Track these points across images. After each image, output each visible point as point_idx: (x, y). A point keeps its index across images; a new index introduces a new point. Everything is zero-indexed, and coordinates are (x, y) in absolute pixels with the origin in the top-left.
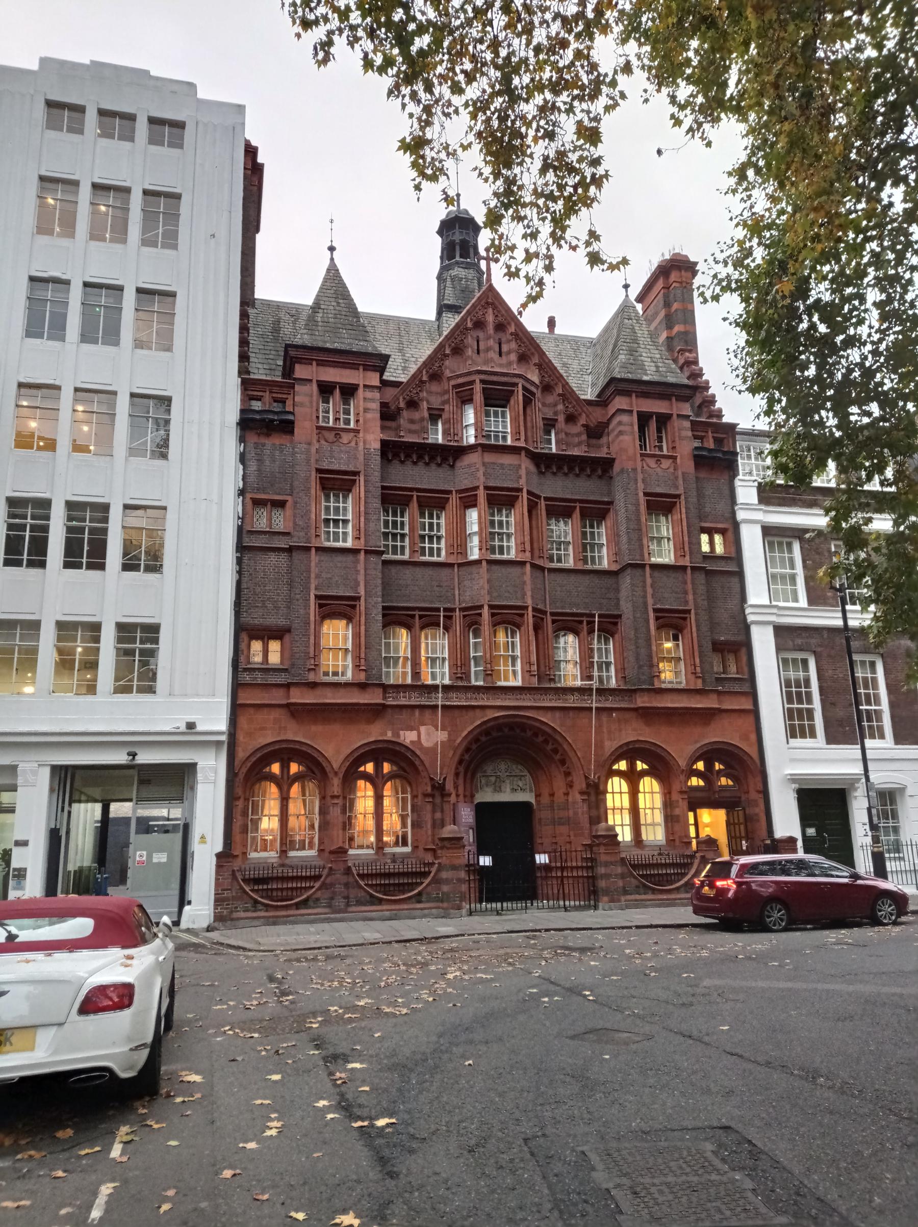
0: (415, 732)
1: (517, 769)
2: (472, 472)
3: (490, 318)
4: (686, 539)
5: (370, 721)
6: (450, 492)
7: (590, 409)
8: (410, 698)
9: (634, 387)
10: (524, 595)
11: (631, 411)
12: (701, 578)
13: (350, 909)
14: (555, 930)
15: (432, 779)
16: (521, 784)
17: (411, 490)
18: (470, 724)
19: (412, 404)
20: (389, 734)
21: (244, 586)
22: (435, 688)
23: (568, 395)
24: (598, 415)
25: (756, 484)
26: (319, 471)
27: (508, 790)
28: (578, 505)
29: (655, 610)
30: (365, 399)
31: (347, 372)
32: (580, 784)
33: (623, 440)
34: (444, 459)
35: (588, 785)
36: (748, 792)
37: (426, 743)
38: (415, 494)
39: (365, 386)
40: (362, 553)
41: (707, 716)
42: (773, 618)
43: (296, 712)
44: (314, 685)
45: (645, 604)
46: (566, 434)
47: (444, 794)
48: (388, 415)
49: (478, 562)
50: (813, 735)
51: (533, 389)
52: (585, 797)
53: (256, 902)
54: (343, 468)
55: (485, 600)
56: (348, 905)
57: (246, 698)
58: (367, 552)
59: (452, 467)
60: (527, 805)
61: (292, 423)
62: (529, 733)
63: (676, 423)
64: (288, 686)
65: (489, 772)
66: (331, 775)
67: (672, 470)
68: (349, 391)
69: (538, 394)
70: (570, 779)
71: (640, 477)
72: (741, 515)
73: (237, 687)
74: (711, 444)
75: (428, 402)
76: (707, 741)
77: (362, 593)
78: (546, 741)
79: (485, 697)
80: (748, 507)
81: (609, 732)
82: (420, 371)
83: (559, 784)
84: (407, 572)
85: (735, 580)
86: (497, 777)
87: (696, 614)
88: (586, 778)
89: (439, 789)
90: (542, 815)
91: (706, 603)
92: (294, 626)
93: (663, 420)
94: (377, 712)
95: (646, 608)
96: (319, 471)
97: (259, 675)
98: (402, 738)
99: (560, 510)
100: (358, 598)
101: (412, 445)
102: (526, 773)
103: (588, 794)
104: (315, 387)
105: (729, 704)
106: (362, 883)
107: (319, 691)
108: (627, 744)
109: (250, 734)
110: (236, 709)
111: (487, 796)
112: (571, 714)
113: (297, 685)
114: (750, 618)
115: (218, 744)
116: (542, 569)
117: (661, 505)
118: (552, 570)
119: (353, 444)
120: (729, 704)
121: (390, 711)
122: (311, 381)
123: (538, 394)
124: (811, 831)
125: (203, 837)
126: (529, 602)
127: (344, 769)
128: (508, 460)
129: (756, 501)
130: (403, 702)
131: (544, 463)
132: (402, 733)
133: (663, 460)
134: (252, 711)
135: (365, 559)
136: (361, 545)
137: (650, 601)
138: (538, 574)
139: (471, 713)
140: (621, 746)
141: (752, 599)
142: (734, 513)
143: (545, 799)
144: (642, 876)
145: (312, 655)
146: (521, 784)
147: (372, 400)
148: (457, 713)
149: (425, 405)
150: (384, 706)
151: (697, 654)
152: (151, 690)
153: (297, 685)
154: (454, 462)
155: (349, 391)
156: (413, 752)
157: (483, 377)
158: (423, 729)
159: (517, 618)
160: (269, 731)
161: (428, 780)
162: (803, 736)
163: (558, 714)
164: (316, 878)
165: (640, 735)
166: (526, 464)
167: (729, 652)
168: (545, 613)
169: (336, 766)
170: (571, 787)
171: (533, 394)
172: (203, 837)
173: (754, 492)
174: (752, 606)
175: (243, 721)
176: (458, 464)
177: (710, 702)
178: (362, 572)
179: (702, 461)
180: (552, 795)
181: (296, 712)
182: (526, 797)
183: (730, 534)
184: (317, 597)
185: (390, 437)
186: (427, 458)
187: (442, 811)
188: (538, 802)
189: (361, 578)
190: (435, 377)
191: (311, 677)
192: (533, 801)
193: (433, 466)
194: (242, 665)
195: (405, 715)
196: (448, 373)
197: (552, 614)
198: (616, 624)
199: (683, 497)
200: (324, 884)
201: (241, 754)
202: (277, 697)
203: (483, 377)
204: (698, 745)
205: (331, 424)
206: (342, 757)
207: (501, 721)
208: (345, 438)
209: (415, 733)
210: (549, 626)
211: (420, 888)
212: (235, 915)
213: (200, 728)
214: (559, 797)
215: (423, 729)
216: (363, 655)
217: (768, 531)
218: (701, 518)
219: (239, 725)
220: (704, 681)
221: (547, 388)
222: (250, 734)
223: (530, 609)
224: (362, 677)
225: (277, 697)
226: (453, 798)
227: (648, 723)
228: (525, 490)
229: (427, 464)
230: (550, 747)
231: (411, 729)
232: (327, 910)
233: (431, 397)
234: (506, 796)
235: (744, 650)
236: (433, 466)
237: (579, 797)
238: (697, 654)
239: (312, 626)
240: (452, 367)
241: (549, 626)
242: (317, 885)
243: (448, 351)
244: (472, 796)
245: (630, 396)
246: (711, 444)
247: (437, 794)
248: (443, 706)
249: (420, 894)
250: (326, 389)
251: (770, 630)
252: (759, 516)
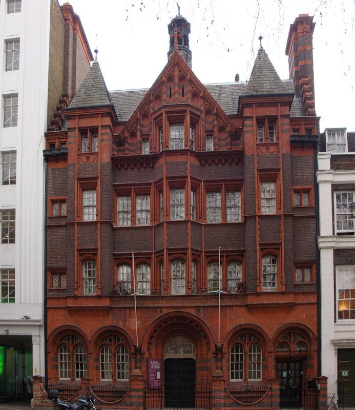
2: (163, 169)
3: (176, 73)
4: (282, 197)
6: (150, 184)
7: (233, 121)
9: (253, 101)
11: (252, 117)
12: (290, 221)
17: (131, 185)
19: (133, 134)
22: (215, 296)
23: (219, 114)
24: (237, 123)
26: (79, 179)
27: (182, 352)
29: (260, 245)
30: (101, 134)
31: (93, 120)
32: (213, 349)
33: (252, 136)
34: (148, 164)
38: (133, 187)
39: (102, 126)
41: (290, 307)
42: (333, 244)
43: (71, 311)
44: (76, 297)
45: (255, 241)
46: (219, 139)
47: (142, 354)
48: (119, 142)
49: (184, 222)
51: (198, 113)
54: (91, 176)
59: (153, 168)
61: (66, 154)
63: (280, 121)
64: (65, 298)
67: (276, 153)
68: (94, 131)
69: (203, 116)
70: (209, 346)
71: (256, 159)
72: (320, 178)
73: (46, 298)
74: (303, 132)
75: (141, 131)
77: (99, 246)
82: (136, 113)
83: (205, 349)
85: (314, 221)
86: (176, 345)
87: (285, 246)
89: (138, 351)
91: (291, 238)
92: (68, 266)
93: (273, 120)
95: (256, 244)
96: (79, 179)
97: (56, 293)
99: (213, 188)
101: (134, 158)
104: (77, 130)
106: (232, 396)
107: (80, 300)
110: (46, 309)
113: (70, 297)
114: (321, 245)
117: (268, 175)
119: (95, 162)
120: (302, 300)
121: (114, 310)
122: (75, 128)
123: (203, 116)
128: (180, 159)
130: (151, 305)
131: (204, 158)
133: (271, 147)
134: (53, 310)
135: (101, 226)
136: (281, 212)
137: (258, 239)
141: (323, 232)
142: (315, 177)
145: (76, 281)
147: (105, 134)
149: (139, 133)
151: (283, 270)
152: (13, 301)
153: (70, 297)
154: (154, 165)
155: (94, 131)
156: (125, 332)
157: (167, 109)
159: (182, 255)
160: (61, 320)
166: (192, 161)
167: (306, 268)
169: (89, 338)
171: (199, 117)
173: (328, 161)
174: (323, 237)
175: (49, 315)
176: (156, 166)
178: (99, 235)
179: (296, 144)
181: (71, 311)
182: (191, 356)
183: (312, 192)
184: (77, 250)
185: (117, 155)
186: (216, 161)
188: (196, 358)
189: (99, 238)
190: (145, 116)
191: (76, 293)
192: (195, 358)
194: (48, 288)
196: (152, 111)
198: (242, 256)
199: (281, 170)
201: (49, 332)
202: (61, 304)
203: (167, 109)
205: (275, 141)
206: (274, 330)
207: (171, 315)
208: (92, 158)
213: (32, 318)
216: (284, 276)
217: (335, 187)
218: (293, 183)
221: (208, 112)
223: (189, 249)
224: (99, 293)
225: (61, 304)
226: (147, 355)
228: (189, 177)
233: (147, 126)
234: (181, 355)
235: (315, 266)
236: (207, 166)
237: (212, 356)
238: (283, 270)
239: (76, 265)
240: (155, 106)
242: (264, 396)
243: (152, 98)
244: (163, 356)
245: (252, 107)
246: (303, 132)
247: (138, 354)
249: (260, 402)
250: (83, 132)
251: (332, 251)
252: (330, 177)
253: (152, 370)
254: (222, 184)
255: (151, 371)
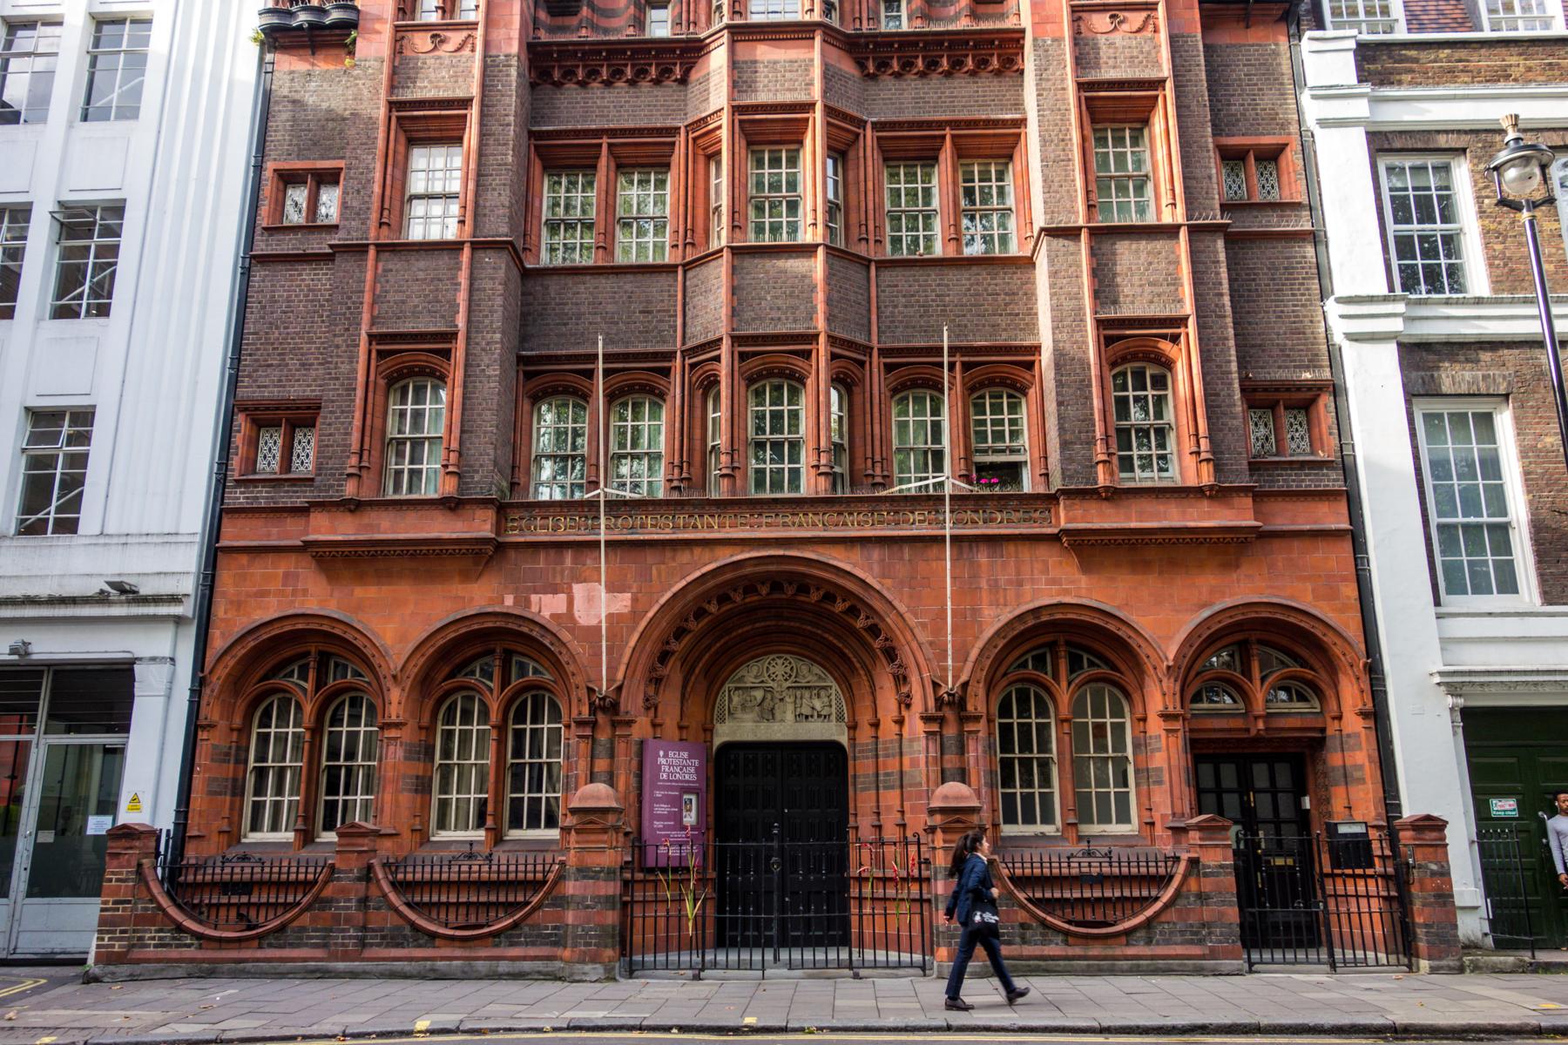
0: (563, 597)
1: (811, 673)
5: (467, 576)
6: (674, 131)
8: (556, 528)
10: (811, 315)
13: (367, 953)
14: (682, 1029)
15: (590, 690)
16: (818, 704)
18: (677, 578)
20: (509, 600)
21: (250, 327)
25: (1352, 44)
27: (790, 716)
28: (948, 132)
35: (939, 702)
36: (1340, 718)
37: (583, 617)
40: (467, 250)
42: (1397, 325)
50: (1508, 585)
52: (935, 728)
53: (180, 928)
55: (722, 329)
56: (363, 944)
57: (235, 534)
58: (476, 246)
60: (835, 746)
62: (790, 591)
64: (303, 511)
65: (750, 680)
66: (389, 683)
76: (1228, 602)
78: (853, 611)
79: (715, 522)
80: (1329, 93)
81: (994, 586)
84: (582, 288)
88: (936, 686)
90: (861, 768)
94: (482, 557)
98: (534, 609)
100: (454, 335)
102: (831, 682)
103: (941, 721)
105: (1288, 517)
108: (1036, 611)
109: (238, 605)
111: (740, 727)
112: (907, 552)
115: (178, 621)
116: (866, 263)
118: (883, 265)
121: (512, 554)
124: (1504, 806)
125: (135, 799)
126: (820, 324)
127: (413, 671)
129: (1352, 78)
132: (534, 598)
134: (244, 559)
138: (855, 273)
139: (684, 557)
140: (1020, 617)
143: (865, 735)
144: (1037, 902)
146: (818, 704)
148: (650, 557)
150: (500, 548)
158: (578, 589)
161: (583, 693)
162: (1481, 588)
163: (876, 553)
164: (307, 885)
165: (1067, 592)
168: (867, 350)
170: (908, 706)
172: (135, 799)
177: (1238, 515)
180: (876, 725)
184: (371, 337)
187: (612, 756)
188: (852, 739)
192: (844, 739)
193: (645, 86)
195: (542, 561)
197: (884, 352)
200: (316, 899)
201: (218, 643)
204: (1206, 613)
209: (562, 598)
210: (876, 378)
211: (1149, 913)
212: (137, 953)
214: (888, 729)
215: (578, 589)
219: (218, 589)
220: (1218, 469)
222: (238, 605)
223: (822, 339)
227: (1086, 567)
229: (632, 83)
230: (860, 624)
231: (555, 590)
232: (319, 953)
234: (785, 729)
235: (1326, 401)
237: (920, 727)
241: (876, 378)
244: (709, 730)
248: (607, 542)
249: (1148, 924)
252: (1360, 108)
253: (660, 788)
254: (944, 137)
255: (658, 794)
